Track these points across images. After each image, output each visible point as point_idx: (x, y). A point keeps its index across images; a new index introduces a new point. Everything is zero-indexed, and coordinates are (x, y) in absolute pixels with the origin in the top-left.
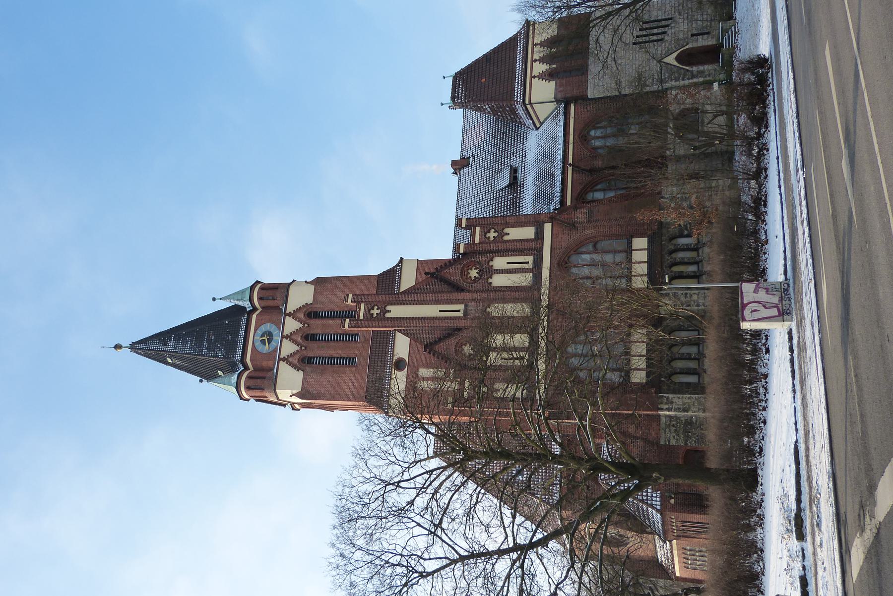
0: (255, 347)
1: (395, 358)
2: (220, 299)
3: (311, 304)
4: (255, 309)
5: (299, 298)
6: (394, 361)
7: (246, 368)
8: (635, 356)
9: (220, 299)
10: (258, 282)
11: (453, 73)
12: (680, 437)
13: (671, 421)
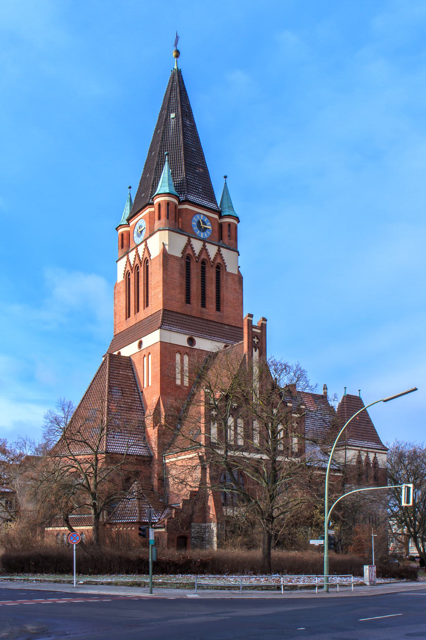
0: (196, 214)
1: (195, 338)
2: (226, 183)
3: (226, 270)
4: (221, 217)
6: (194, 337)
7: (181, 203)
8: (346, 452)
9: (226, 183)
11: (362, 397)
12: (196, 534)
13: (203, 529)
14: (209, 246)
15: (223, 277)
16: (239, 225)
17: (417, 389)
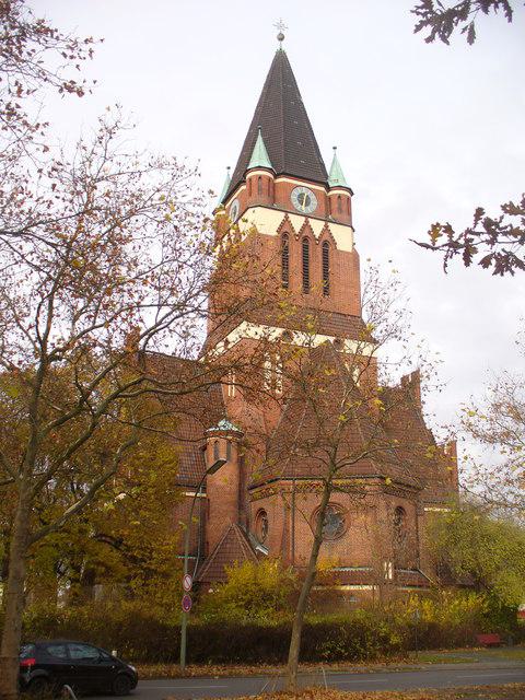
5: (339, 234)
7: (276, 176)
8: (315, 556)
10: (352, 194)
14: (313, 222)
15: (332, 260)
16: (352, 198)
17: (448, 43)
